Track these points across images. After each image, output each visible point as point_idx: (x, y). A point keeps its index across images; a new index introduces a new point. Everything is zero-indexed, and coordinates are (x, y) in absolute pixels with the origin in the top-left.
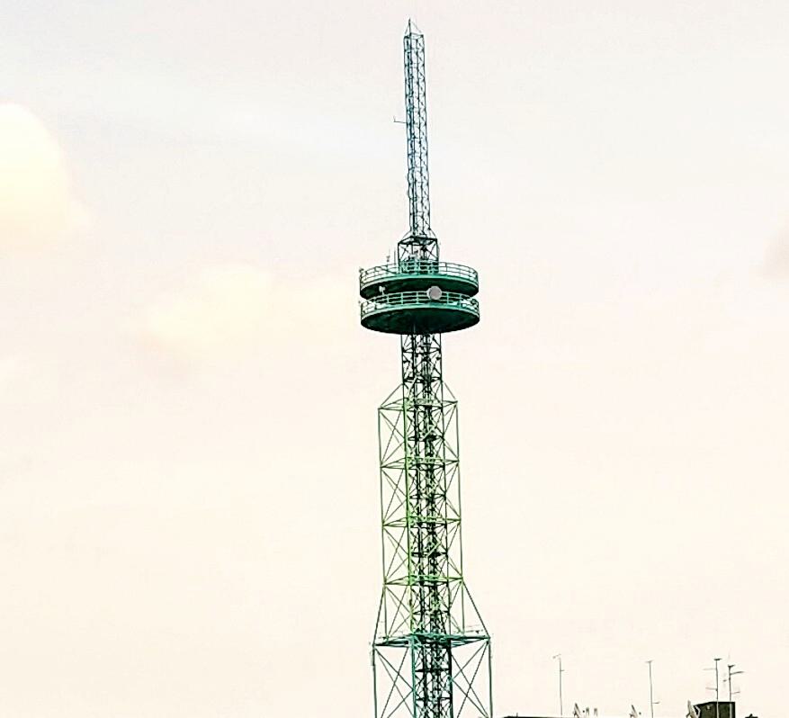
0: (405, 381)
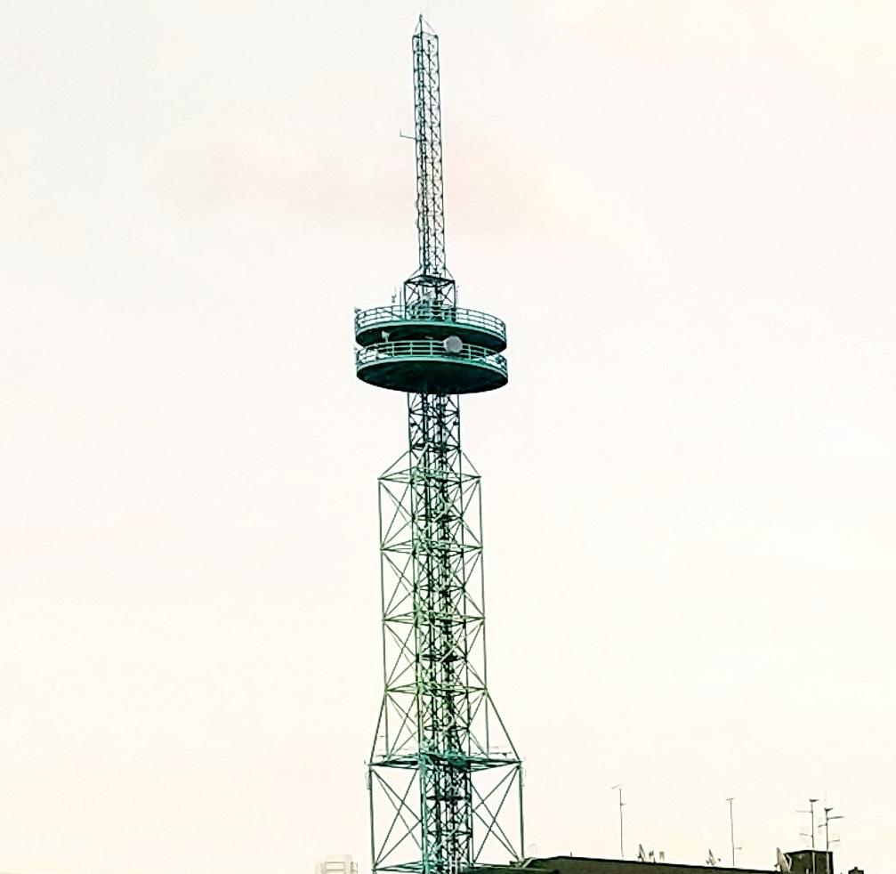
0: (412, 448)
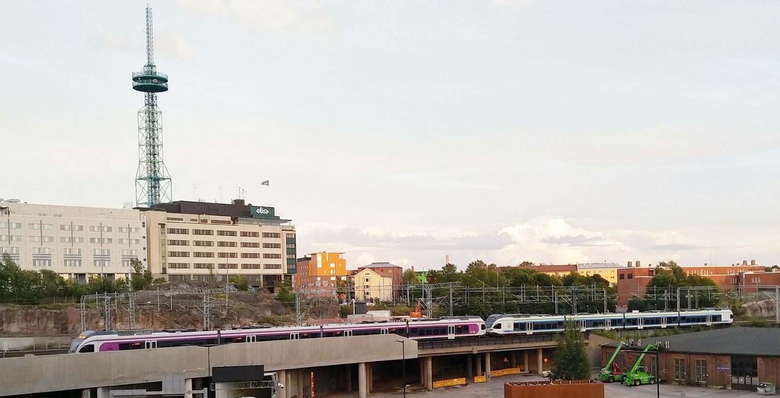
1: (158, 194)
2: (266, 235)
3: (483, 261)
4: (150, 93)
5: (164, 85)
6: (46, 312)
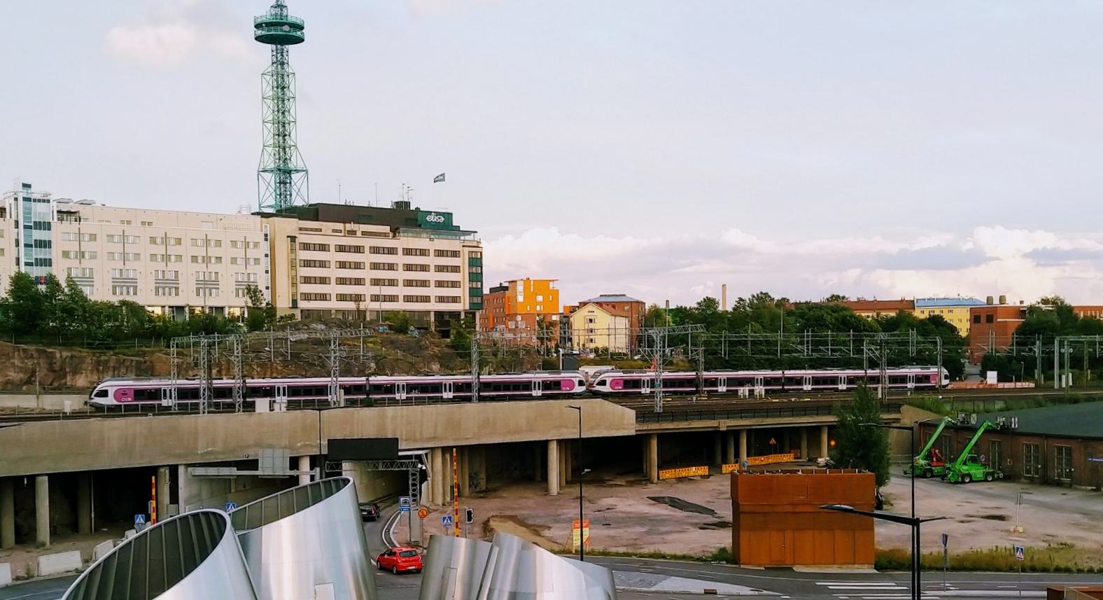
0: (273, 63)
1: (288, 193)
2: (440, 253)
3: (770, 294)
4: (279, 46)
5: (299, 33)
6: (124, 360)
